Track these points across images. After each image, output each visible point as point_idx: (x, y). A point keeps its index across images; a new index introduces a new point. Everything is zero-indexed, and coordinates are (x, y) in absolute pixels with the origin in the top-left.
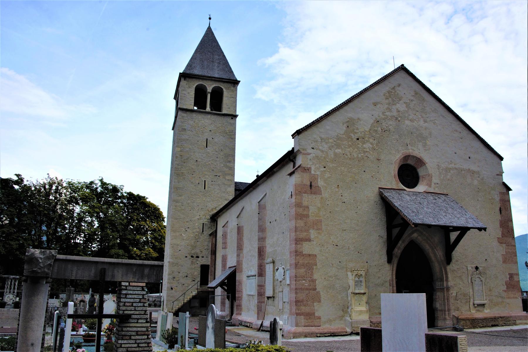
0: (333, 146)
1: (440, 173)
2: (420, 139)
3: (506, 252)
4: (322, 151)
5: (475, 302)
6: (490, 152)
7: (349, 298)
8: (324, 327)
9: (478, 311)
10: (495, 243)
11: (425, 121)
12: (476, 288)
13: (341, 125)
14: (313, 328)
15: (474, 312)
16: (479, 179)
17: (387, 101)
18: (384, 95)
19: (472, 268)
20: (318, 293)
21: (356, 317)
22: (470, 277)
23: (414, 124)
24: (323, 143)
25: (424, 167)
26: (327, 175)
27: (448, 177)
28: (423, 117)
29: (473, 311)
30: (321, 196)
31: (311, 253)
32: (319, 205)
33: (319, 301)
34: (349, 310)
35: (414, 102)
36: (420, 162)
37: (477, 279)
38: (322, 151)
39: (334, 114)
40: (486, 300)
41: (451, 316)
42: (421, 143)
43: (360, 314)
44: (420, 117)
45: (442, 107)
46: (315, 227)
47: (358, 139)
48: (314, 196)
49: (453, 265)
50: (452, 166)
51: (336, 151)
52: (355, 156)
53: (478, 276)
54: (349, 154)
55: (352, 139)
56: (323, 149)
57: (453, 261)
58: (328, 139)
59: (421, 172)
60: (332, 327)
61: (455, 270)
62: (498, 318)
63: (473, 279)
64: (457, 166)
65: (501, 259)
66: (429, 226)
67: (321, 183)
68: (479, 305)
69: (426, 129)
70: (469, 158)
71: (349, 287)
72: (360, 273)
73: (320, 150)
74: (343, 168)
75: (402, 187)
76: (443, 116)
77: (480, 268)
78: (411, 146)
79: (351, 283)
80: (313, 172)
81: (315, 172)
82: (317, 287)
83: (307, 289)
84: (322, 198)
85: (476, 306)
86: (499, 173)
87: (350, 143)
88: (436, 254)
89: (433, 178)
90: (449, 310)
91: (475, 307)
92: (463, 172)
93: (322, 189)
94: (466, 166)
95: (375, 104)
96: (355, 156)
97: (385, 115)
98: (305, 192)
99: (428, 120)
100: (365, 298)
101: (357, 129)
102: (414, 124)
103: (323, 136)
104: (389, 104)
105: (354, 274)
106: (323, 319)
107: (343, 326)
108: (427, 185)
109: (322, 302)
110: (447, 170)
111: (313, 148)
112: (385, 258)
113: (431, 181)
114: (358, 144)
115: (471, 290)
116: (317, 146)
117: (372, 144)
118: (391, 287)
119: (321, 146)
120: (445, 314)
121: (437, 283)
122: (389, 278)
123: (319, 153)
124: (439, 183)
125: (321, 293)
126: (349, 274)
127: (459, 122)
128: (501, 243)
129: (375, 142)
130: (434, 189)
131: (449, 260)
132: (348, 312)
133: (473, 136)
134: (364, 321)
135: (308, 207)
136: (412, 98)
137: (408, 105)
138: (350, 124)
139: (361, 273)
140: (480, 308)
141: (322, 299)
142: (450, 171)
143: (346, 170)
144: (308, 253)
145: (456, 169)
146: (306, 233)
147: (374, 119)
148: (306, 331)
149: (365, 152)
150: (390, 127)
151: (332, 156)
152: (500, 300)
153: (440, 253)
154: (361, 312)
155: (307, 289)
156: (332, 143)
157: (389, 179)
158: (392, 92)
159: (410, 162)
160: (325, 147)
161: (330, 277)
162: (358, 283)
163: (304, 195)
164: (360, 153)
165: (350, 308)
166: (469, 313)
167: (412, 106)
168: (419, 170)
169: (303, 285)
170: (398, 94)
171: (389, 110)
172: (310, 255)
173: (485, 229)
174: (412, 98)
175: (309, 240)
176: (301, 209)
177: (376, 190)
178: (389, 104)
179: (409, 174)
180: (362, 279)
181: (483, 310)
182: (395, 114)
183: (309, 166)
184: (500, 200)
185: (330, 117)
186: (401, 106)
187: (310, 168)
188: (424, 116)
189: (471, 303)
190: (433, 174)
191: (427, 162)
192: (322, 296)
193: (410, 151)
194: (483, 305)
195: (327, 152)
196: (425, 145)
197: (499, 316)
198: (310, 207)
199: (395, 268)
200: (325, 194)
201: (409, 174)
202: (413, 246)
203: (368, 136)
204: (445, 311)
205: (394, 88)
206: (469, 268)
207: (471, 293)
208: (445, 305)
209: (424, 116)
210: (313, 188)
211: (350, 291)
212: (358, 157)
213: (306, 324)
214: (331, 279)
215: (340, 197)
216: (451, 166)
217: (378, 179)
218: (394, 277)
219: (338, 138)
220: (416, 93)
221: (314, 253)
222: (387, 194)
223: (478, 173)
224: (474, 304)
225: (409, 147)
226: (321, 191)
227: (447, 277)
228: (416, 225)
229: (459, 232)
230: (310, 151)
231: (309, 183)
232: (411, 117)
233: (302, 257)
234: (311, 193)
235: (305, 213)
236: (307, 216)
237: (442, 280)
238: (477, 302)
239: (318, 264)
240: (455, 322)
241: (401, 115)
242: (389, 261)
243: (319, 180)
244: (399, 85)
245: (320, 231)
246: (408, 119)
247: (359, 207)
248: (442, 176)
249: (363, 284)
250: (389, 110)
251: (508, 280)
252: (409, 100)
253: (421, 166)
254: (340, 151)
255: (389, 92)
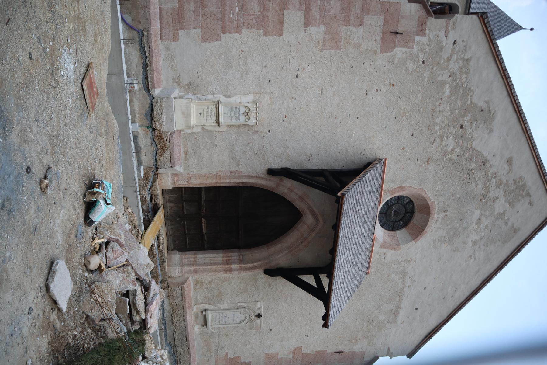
0: (454, 80)
1: (399, 263)
2: (452, 232)
3: (281, 358)
4: (449, 60)
5: (209, 312)
6: (421, 339)
7: (210, 96)
8: (161, 47)
9: (197, 317)
10: (293, 344)
11: (474, 243)
12: (229, 314)
13: (486, 99)
14: (158, 25)
15: (195, 310)
16: (386, 322)
17: (511, 182)
18: (521, 178)
19: (260, 308)
20: (218, 38)
21: (178, 106)
22: (245, 305)
23: (474, 224)
24: (461, 62)
25: (410, 238)
26: (411, 66)
27: (393, 276)
28: (481, 239)
29: (195, 309)
30: (378, 51)
31: (285, 25)
32: (364, 47)
33: (204, 40)
34: (190, 96)
35: (504, 226)
36: (418, 232)
37: (243, 316)
38: (449, 60)
39: (504, 87)
40: (213, 328)
41: (187, 275)
42: (445, 234)
43: (183, 113)
44: (483, 235)
45: (492, 270)
46: (327, 37)
47: (462, 127)
48: (379, 38)
49: (263, 280)
50: (408, 283)
51: (447, 86)
52: (437, 120)
53: (247, 317)
54: (441, 108)
55: (463, 116)
56: (452, 62)
57: (270, 279)
58: (467, 73)
59: (401, 234)
60: (161, 63)
61: (256, 282)
62: (188, 345)
63: (243, 310)
64: (406, 289)
65: (272, 351)
66: (336, 227)
67: (400, 52)
68: (205, 317)
69: (465, 243)
70: (416, 309)
71: (229, 97)
72: (253, 116)
73: (451, 56)
74: (420, 95)
75: (386, 198)
76: (478, 271)
77: (258, 321)
78: (443, 218)
79: (236, 100)
80: (417, 38)
81: (418, 44)
82: (228, 35)
83: (224, 15)
84: (375, 52)
85: (204, 313)
86: (391, 351)
87: (457, 111)
88: (281, 253)
89: (393, 251)
90: (195, 272)
91: (202, 312)
92: (398, 299)
93: (389, 54)
94: (405, 303)
95: (509, 161)
96: (437, 120)
97: (492, 176)
98: (386, 21)
99: (476, 248)
100: (211, 122)
101: (477, 127)
102: (474, 224)
103: (472, 63)
104: (507, 185)
105: (250, 105)
106: (173, 45)
107: (164, 83)
108: (384, 242)
109: (204, 44)
110: (403, 275)
111: (455, 43)
112: (276, 164)
113: (390, 247)
114: (454, 127)
115: (226, 306)
116: (459, 51)
117: (453, 150)
118: (229, 174)
119: (457, 59)
120: (189, 265)
121: (236, 254)
122: (243, 170)
123: (446, 55)
124: (386, 261)
125: (217, 44)
126: (250, 98)
127: (467, 295)
128: (294, 352)
129: (455, 157)
130: (378, 253)
131: (271, 272)
132: (187, 93)
133: (445, 316)
134: (172, 120)
135: (361, 24)
136: (510, 224)
137: (501, 215)
138: (486, 115)
139: (252, 119)
140: (201, 319)
141: (208, 44)
142: (401, 278)
143: (416, 101)
144: (286, 21)
145: (403, 288)
146: (318, 18)
147: (488, 158)
148: (152, 8)
149: (442, 137)
150: (473, 184)
151: (440, 78)
152: (213, 349)
153: (282, 260)
154: (187, 115)
155: (224, 15)
156: (460, 79)
157: (399, 178)
158: (523, 191)
159: (417, 217)
160: (455, 66)
161: (245, 62)
162: (233, 110)
163: (382, 18)
164: (440, 129)
165: (193, 97)
166: (193, 303)
167: (499, 222)
168: (404, 230)
169: (232, 8)
170: (519, 201)
171: (498, 186)
172: (281, 23)
173: (325, 325)
174: (510, 224)
175: (307, 24)
176: (358, 12)
177: (382, 154)
178: (507, 185)
179: (402, 215)
180: (242, 119)
181: (197, 324)
182: (493, 193)
183: (427, 32)
184: (355, 352)
185: (501, 79)
186: (500, 205)
187: (424, 35)
188: (483, 242)
189: (207, 306)
190: (399, 251)
191: (418, 242)
192: (212, 45)
193: (436, 216)
194: (205, 324)
195: (446, 68)
196: (442, 240)
197: (191, 346)
198: (361, 29)
199: (258, 181)
200: (381, 60)
201: (402, 215)
202: (294, 216)
203: (465, 145)
204: (194, 265)
205: (528, 195)
206: (259, 305)
207: (222, 307)
208: (204, 264)
209: (483, 242)
210: (393, 36)
211: (222, 99)
212: (435, 124)
213: (164, 13)
214: (241, 62)
215: (375, 88)
216: (408, 280)
217: (399, 157)
218: (245, 180)
219: (468, 91)
220: (516, 231)
221: (285, 32)
222: (369, 177)
223: (395, 321)
224: (205, 310)
225: (442, 215)
226: (386, 52)
227: (245, 269)
228: (339, 202)
229: (316, 286)
230: (452, 36)
231: (400, 29)
232: (483, 219)
233: (278, 9)
234: (384, 33)
235: (352, 18)
236: (347, 23)
237: (241, 261)
238: (209, 315)
239: (266, 39)
240: (179, 280)
241: (489, 204)
242: (271, 172)
243: (404, 50)
244: (531, 204)
245: (321, 46)
246: (481, 215)
247: (358, 121)
248: (395, 266)
249: (234, 122)
250: (498, 186)
251: (243, 361)
252: (508, 219)
253: (411, 234)
254: (447, 93)
255: (524, 185)
